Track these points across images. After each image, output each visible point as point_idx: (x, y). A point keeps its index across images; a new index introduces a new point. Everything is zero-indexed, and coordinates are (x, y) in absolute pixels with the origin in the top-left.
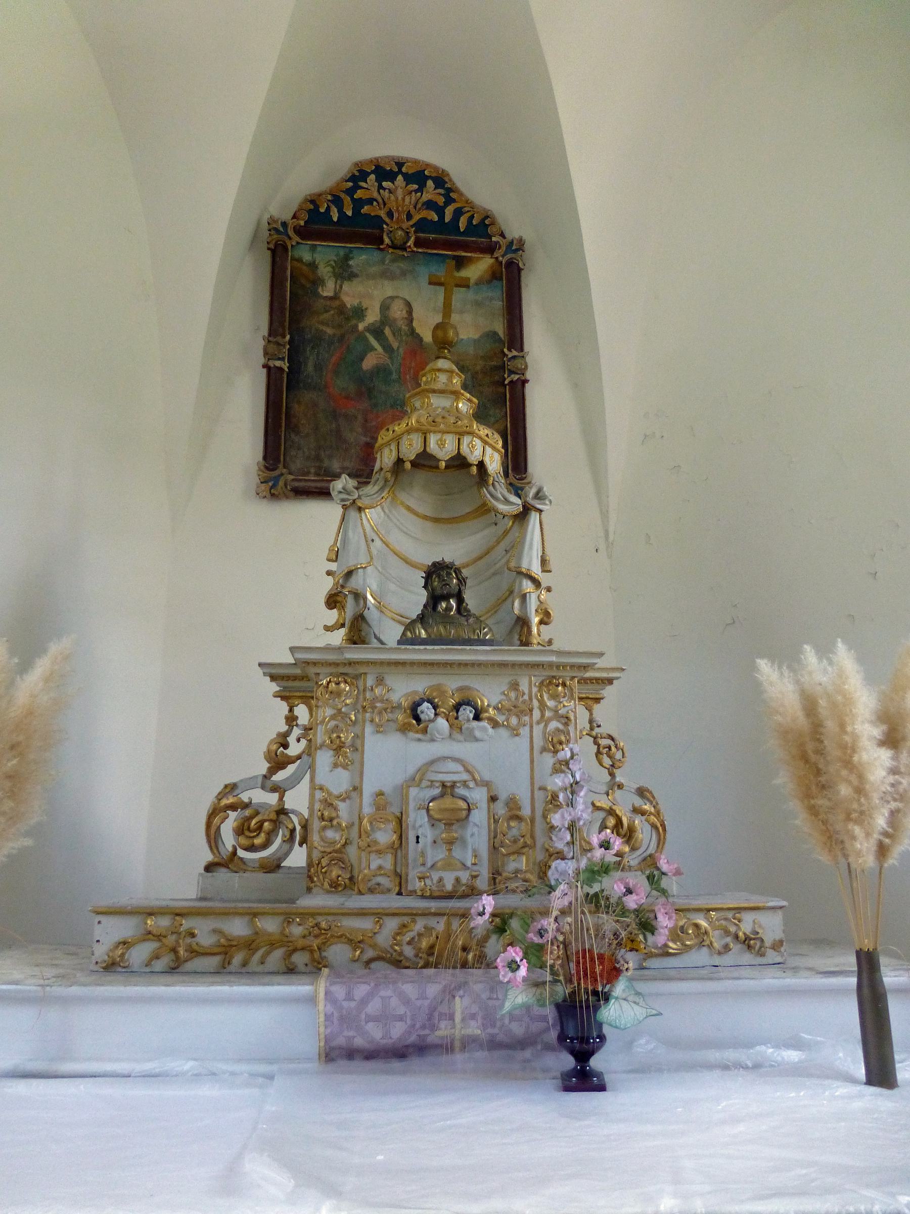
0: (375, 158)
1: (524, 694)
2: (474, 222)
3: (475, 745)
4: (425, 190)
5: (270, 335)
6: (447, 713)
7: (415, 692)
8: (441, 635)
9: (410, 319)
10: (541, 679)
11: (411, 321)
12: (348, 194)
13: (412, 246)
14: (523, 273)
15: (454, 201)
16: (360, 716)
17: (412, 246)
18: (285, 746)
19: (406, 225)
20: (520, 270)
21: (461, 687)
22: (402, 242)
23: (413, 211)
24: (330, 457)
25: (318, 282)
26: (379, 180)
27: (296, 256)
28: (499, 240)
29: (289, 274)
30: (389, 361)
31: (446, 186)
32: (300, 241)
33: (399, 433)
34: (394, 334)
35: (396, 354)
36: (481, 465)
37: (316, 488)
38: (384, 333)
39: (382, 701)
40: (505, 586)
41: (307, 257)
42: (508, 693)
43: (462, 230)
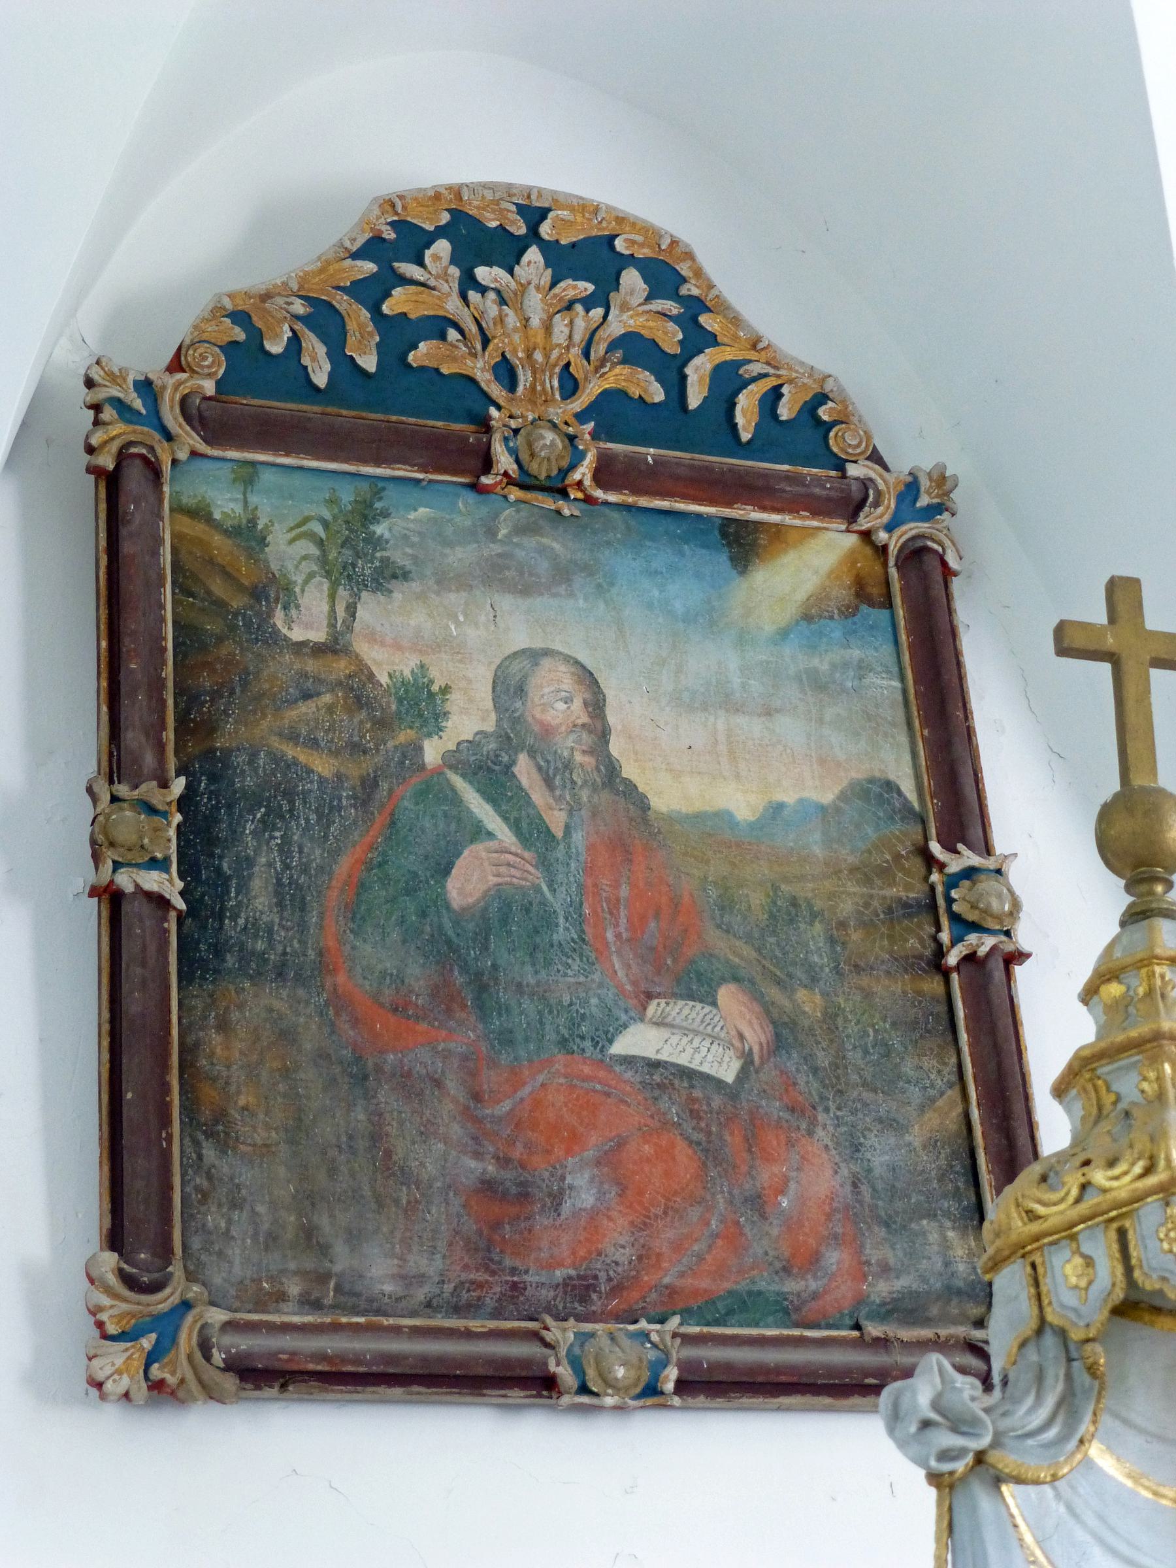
0: (449, 188)
11: (604, 735)
13: (587, 482)
14: (956, 584)
15: (712, 340)
17: (587, 482)
19: (562, 411)
22: (554, 473)
23: (579, 368)
24: (354, 1238)
28: (873, 475)
30: (536, 876)
31: (683, 291)
32: (202, 447)
34: (549, 782)
35: (560, 852)
37: (323, 1357)
38: (514, 776)
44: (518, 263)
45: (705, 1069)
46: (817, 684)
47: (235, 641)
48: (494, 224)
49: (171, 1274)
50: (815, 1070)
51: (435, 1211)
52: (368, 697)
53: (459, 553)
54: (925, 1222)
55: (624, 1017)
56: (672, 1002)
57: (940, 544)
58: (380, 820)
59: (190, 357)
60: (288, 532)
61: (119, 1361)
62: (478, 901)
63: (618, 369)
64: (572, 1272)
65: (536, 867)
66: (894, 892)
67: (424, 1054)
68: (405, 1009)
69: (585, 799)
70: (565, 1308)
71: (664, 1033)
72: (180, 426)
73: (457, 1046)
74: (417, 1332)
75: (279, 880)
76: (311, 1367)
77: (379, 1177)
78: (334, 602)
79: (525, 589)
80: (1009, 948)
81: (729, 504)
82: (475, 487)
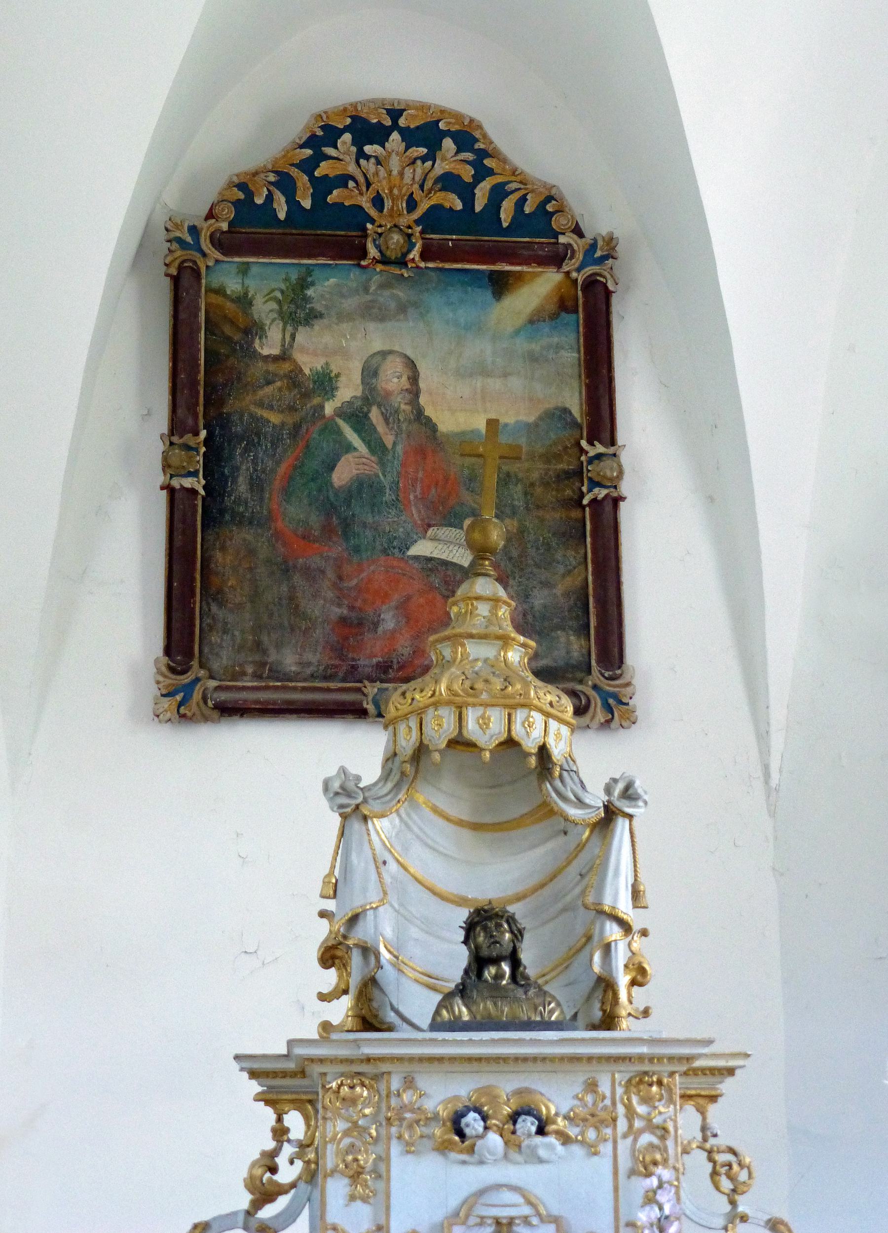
1: (604, 1098)
2: (527, 210)
3: (540, 1168)
4: (439, 155)
5: (172, 432)
6: (501, 1125)
7: (456, 1098)
8: (490, 1014)
9: (414, 391)
10: (627, 1076)
12: (304, 172)
14: (614, 299)
15: (490, 172)
16: (383, 1132)
17: (417, 259)
18: (273, 1169)
20: (608, 294)
21: (519, 1089)
22: (400, 255)
24: (279, 646)
25: (252, 330)
26: (359, 142)
27: (215, 285)
29: (203, 318)
30: (377, 469)
31: (476, 147)
33: (421, 705)
34: (386, 420)
36: (543, 752)
37: (257, 702)
38: (369, 418)
39: (412, 1111)
40: (580, 930)
41: (233, 286)
42: (583, 1096)
43: (505, 225)
44: (387, 141)
45: (455, 560)
46: (533, 358)
47: (235, 357)
48: (375, 121)
49: (192, 665)
50: (510, 559)
51: (318, 633)
52: (299, 381)
53: (350, 301)
54: (559, 632)
55: (415, 537)
56: (440, 528)
57: (604, 277)
58: (301, 444)
59: (217, 210)
60: (264, 297)
61: (166, 706)
62: (347, 483)
63: (438, 194)
64: (381, 659)
65: (376, 464)
66: (561, 466)
67: (317, 559)
68: (309, 537)
69: (404, 428)
70: (376, 676)
71: (436, 544)
72: (210, 249)
73: (333, 554)
74: (304, 689)
75: (251, 477)
76: (253, 706)
77: (292, 617)
78: (284, 332)
79: (382, 318)
80: (615, 495)
81: (493, 263)
82: (359, 265)
